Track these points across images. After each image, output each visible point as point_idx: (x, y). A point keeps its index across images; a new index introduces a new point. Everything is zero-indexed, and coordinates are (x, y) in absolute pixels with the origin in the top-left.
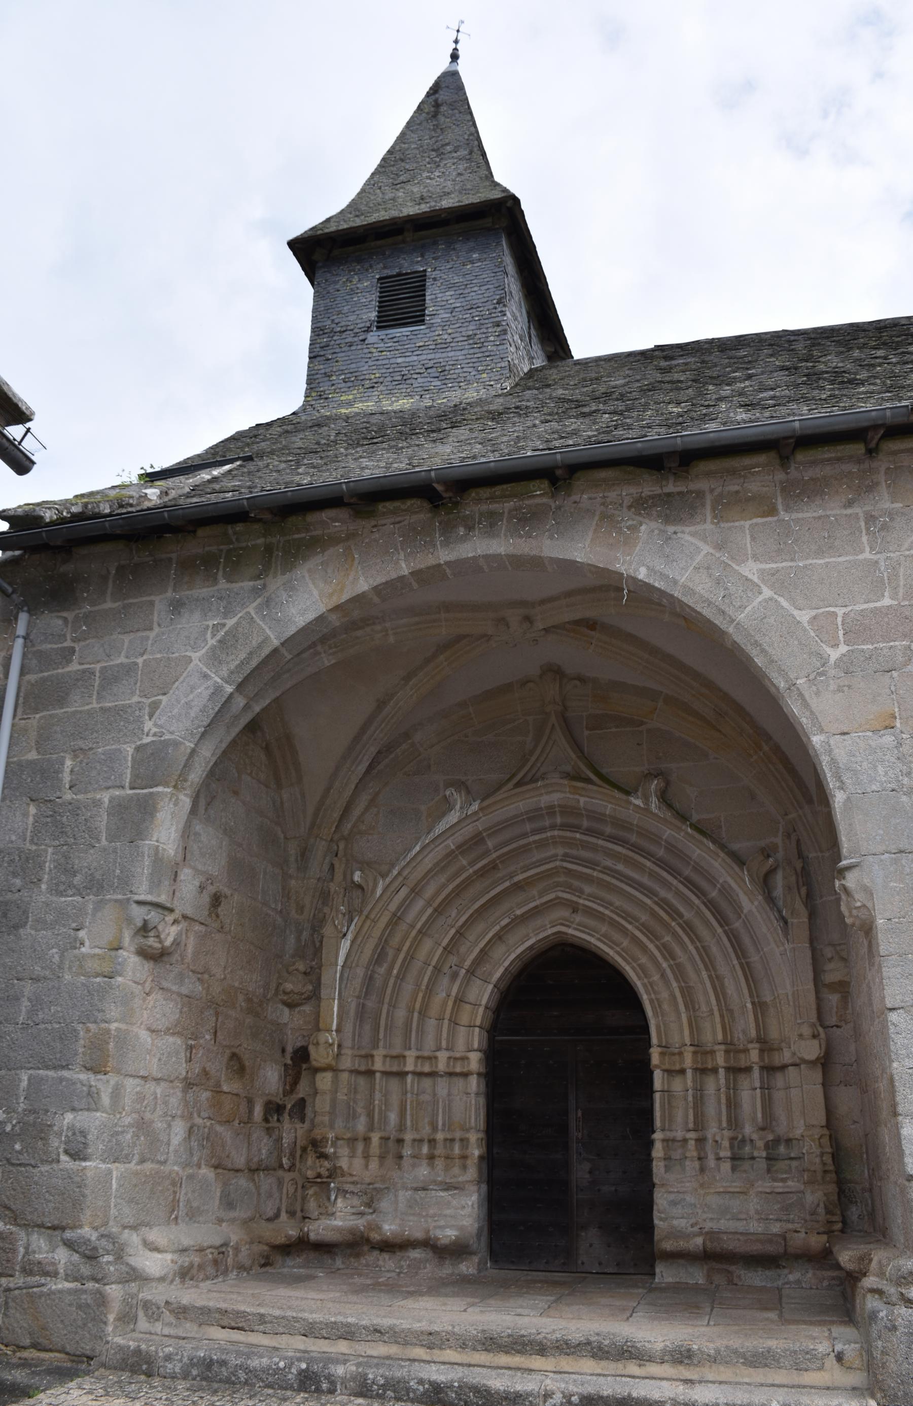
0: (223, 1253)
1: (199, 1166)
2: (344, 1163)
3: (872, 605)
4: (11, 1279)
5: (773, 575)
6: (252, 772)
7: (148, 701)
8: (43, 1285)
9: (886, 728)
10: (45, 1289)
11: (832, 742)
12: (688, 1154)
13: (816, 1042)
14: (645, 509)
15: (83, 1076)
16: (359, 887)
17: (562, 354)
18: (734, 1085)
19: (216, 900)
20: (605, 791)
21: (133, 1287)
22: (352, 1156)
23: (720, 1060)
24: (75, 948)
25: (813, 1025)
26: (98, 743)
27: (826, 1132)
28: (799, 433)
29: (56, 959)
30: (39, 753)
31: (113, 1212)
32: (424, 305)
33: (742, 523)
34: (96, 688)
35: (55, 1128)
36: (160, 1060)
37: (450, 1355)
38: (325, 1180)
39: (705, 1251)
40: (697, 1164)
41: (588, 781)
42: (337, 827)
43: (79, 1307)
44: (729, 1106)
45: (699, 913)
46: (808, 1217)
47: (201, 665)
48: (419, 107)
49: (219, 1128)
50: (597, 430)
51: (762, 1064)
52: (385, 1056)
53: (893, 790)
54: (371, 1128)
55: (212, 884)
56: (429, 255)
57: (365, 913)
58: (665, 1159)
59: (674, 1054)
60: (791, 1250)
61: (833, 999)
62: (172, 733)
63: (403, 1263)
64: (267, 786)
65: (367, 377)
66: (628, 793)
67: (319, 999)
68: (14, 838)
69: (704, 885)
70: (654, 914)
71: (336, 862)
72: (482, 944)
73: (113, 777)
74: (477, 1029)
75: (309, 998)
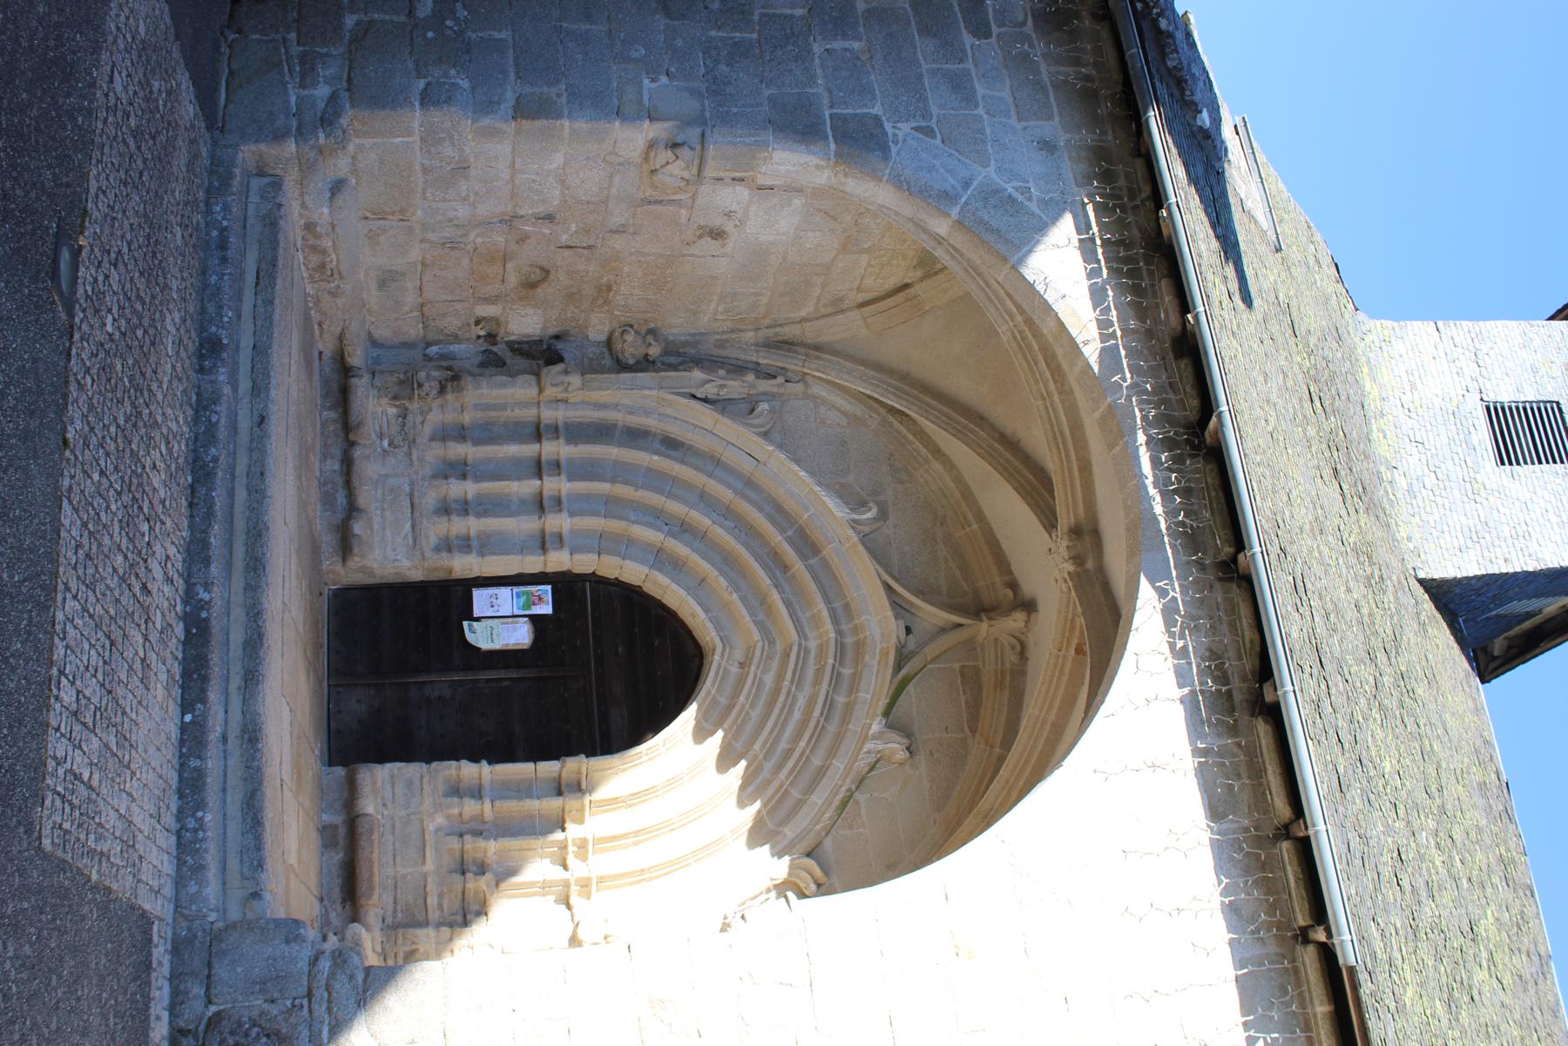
6: (872, 266)
7: (933, 124)
8: (291, 75)
10: (287, 78)
20: (886, 688)
26: (880, 74)
29: (635, 55)
30: (864, 12)
36: (534, 181)
38: (416, 392)
41: (898, 667)
47: (979, 179)
55: (736, 226)
58: (463, 873)
62: (898, 153)
64: (859, 288)
66: (886, 713)
67: (619, 372)
73: (842, 94)
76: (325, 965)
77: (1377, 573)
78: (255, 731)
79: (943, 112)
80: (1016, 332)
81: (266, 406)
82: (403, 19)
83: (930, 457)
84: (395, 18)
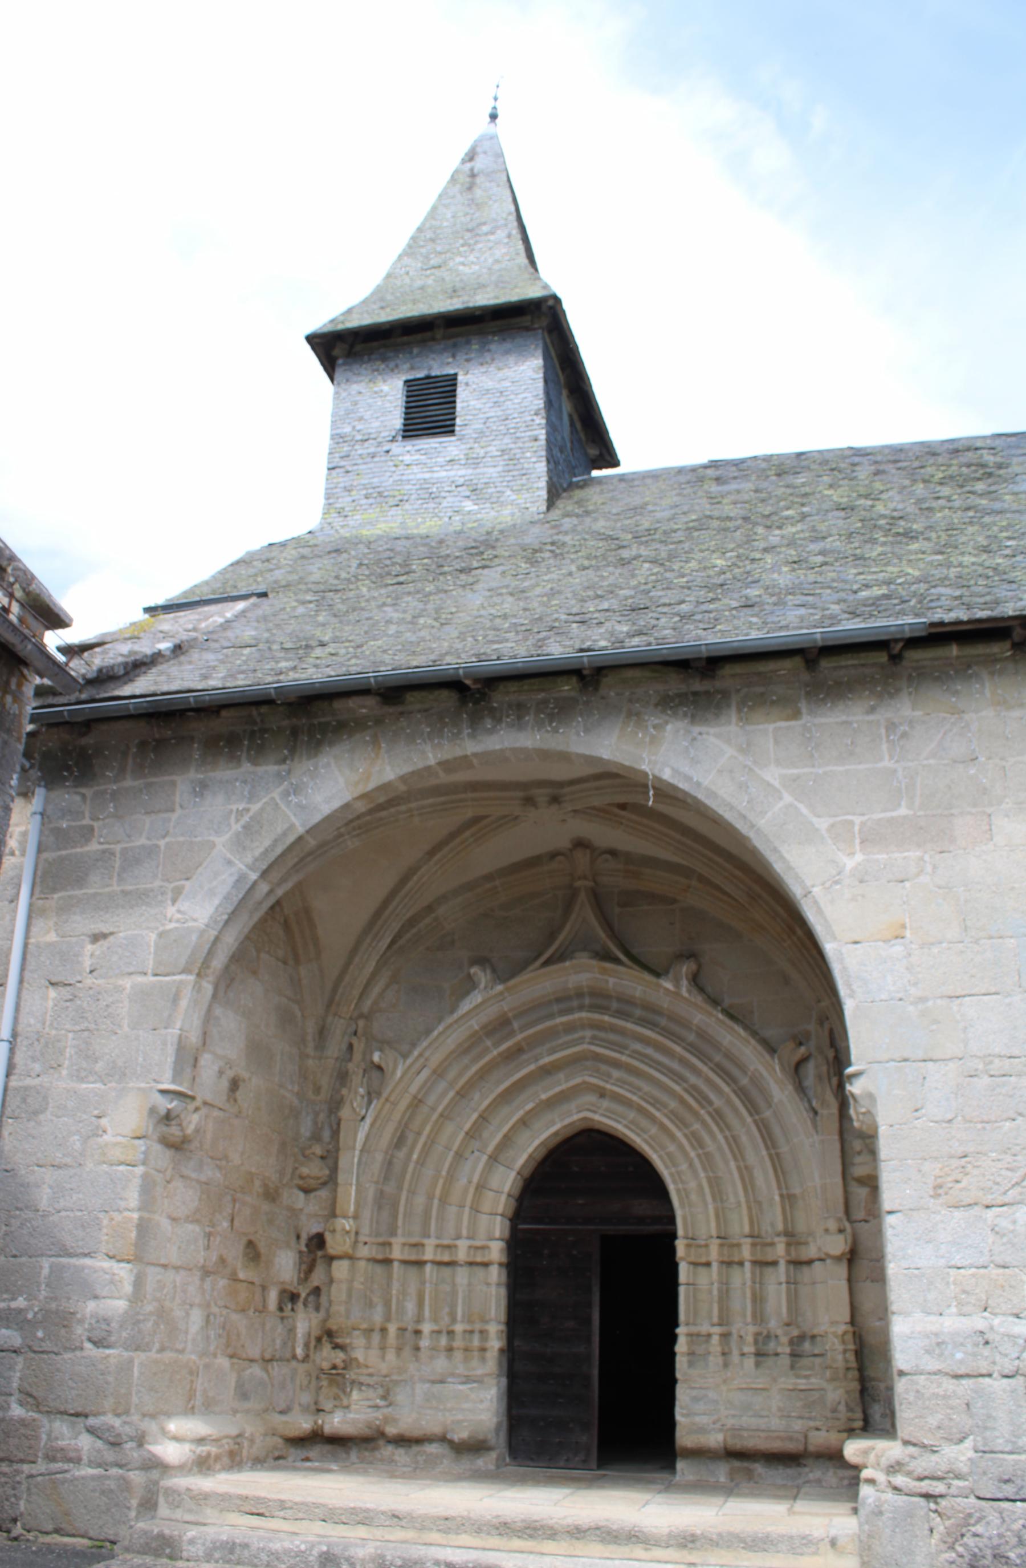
0: (238, 1444)
1: (215, 1355)
2: (359, 1354)
3: (889, 814)
4: (33, 1465)
5: (794, 780)
8: (66, 1471)
9: (897, 937)
10: (68, 1475)
11: (844, 950)
12: (712, 1349)
13: (841, 1238)
14: (671, 708)
15: (107, 1264)
16: (379, 1068)
17: (608, 458)
18: (761, 1279)
19: (235, 1084)
21: (155, 1474)
22: (368, 1347)
23: (746, 1253)
24: (98, 1136)
25: (839, 1220)
27: (849, 1328)
28: (820, 644)
29: (78, 1146)
30: (58, 935)
31: (135, 1399)
32: (454, 413)
33: (766, 726)
34: (117, 870)
35: (79, 1316)
36: (179, 1248)
37: (465, 1539)
38: (340, 1371)
39: (725, 1448)
40: (720, 1360)
41: (617, 961)
42: (356, 1004)
43: (103, 1492)
44: (754, 1300)
45: (729, 1102)
46: (829, 1415)
48: (452, 176)
49: (235, 1317)
50: (635, 588)
51: (788, 1258)
52: (404, 1244)
53: (901, 1000)
54: (388, 1319)
56: (461, 357)
57: (385, 1095)
58: (689, 1354)
59: (700, 1246)
60: (811, 1448)
61: (862, 1192)
63: (419, 1458)
65: (391, 493)
66: (658, 975)
67: (336, 1184)
68: (32, 1021)
69: (735, 1072)
70: (682, 1101)
71: (355, 1041)
72: (506, 1129)
74: (499, 1218)
75: (325, 1184)
76: (899, 1480)
77: (549, 547)
78: (684, 1538)
79: (160, 876)
80: (355, 833)
81: (383, 1513)
82: (20, 1359)
83: (433, 915)
84: (19, 1367)
